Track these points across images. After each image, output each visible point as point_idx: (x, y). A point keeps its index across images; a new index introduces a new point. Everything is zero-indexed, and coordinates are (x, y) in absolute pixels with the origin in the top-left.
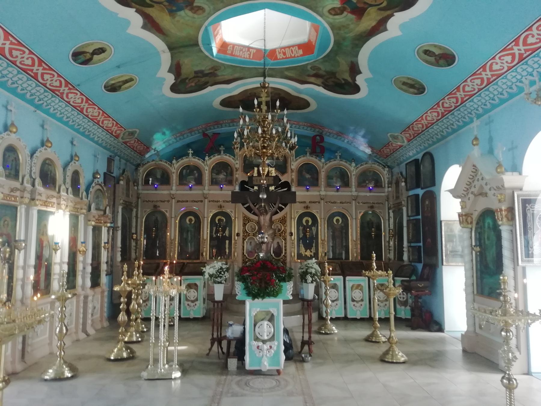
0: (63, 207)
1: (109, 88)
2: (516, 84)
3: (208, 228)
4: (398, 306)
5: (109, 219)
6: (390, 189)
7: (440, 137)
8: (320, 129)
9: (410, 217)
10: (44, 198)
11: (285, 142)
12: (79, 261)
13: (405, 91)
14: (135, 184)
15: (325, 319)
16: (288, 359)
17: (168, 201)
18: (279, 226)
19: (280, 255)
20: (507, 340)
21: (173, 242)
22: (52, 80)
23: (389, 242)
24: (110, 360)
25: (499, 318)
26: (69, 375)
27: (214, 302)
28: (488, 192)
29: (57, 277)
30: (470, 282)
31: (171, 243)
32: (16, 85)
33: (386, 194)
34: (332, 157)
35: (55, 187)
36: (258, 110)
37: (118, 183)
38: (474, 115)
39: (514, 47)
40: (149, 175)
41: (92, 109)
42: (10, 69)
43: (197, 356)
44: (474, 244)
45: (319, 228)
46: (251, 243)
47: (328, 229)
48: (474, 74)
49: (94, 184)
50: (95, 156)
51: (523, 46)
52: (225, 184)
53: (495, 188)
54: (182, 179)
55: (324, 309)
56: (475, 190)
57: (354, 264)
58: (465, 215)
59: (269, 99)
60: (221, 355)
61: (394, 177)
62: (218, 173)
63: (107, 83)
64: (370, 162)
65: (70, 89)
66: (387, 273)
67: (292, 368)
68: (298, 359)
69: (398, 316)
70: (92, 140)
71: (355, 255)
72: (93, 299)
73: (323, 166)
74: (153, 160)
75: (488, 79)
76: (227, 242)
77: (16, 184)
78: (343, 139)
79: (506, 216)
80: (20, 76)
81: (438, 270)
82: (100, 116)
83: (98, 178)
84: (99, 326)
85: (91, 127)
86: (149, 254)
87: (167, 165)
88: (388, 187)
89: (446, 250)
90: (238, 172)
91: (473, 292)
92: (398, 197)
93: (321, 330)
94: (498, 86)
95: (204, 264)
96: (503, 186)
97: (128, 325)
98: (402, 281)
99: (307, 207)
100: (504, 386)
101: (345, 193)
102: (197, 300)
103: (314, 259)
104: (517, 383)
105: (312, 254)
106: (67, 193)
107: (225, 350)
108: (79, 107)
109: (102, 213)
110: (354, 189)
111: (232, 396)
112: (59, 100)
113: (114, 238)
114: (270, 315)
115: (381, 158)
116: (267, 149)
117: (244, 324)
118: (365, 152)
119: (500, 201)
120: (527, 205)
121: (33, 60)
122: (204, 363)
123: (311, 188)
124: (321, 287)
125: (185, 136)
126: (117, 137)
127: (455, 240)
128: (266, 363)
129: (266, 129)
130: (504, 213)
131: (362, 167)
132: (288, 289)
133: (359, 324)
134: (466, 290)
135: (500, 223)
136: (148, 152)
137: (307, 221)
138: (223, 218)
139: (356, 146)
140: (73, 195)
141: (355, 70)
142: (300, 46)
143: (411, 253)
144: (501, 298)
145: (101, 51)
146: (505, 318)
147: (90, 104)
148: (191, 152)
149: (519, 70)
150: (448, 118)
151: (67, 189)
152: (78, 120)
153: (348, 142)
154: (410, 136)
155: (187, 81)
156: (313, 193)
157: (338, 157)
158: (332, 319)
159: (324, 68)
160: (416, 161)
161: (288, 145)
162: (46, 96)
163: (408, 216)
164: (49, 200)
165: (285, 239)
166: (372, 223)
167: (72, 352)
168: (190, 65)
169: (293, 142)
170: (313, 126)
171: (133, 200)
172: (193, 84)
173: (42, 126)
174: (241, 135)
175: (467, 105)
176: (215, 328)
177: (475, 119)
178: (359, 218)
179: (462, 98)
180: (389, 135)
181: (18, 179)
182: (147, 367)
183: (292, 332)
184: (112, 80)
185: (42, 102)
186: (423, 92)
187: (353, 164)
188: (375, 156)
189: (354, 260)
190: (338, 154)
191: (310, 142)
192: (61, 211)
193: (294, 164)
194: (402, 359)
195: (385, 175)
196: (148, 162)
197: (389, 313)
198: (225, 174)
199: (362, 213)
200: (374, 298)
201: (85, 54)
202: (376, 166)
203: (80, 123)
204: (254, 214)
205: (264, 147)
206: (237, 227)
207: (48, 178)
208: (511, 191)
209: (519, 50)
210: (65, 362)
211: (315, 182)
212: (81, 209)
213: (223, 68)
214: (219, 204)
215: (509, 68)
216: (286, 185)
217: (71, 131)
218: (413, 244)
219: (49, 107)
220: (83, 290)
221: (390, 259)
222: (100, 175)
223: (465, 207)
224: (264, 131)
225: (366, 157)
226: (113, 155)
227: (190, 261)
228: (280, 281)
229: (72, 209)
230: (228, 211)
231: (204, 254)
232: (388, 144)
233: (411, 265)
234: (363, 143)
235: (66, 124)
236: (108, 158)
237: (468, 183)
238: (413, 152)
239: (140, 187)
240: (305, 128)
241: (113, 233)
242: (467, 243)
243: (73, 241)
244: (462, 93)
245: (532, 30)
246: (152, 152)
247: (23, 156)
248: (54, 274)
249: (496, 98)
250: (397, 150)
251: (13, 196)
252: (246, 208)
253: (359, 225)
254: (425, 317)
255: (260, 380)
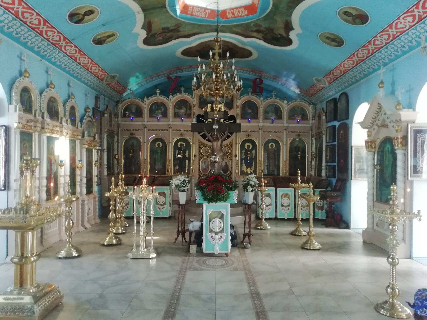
0: (65, 134)
1: (96, 42)
2: (415, 39)
3: (172, 151)
4: (316, 210)
5: (98, 143)
6: (313, 121)
7: (354, 80)
8: (260, 73)
9: (328, 143)
10: (51, 127)
11: (233, 85)
12: (77, 175)
13: (328, 44)
14: (116, 117)
15: (261, 219)
16: (233, 246)
17: (142, 130)
18: (227, 149)
19: (227, 172)
20: (392, 232)
21: (146, 161)
22: (53, 36)
23: (311, 162)
24: (103, 245)
25: (388, 215)
26: (76, 255)
27: (179, 205)
28: (389, 124)
29: (62, 186)
30: (371, 192)
31: (144, 162)
32: (27, 40)
33: (310, 125)
34: (269, 96)
35: (58, 119)
36: (213, 60)
37: (103, 116)
38: (382, 63)
39: (415, 10)
40: (126, 110)
41: (83, 58)
42: (22, 28)
43: (167, 243)
44: (376, 164)
45: (258, 151)
46: (205, 162)
47: (264, 152)
48: (383, 31)
49: (86, 117)
50: (86, 95)
51: (422, 9)
52: (185, 117)
53: (394, 121)
54: (152, 113)
55: (260, 211)
56: (379, 123)
57: (284, 178)
58: (370, 142)
59: (221, 51)
60: (184, 243)
61: (317, 112)
62: (180, 108)
63: (94, 38)
64: (299, 100)
65: (67, 43)
66: (309, 185)
67: (237, 252)
68: (241, 246)
69: (316, 217)
70: (83, 82)
71: (285, 172)
72: (88, 202)
73: (262, 103)
74: (129, 98)
75: (394, 35)
76: (187, 161)
77: (31, 117)
78: (277, 81)
79: (401, 143)
80: (30, 33)
81: (348, 183)
82: (89, 64)
83: (89, 112)
84: (93, 223)
85: (82, 72)
86: (127, 170)
87: (140, 102)
88: (312, 120)
89: (355, 168)
90: (195, 108)
91: (373, 199)
92: (319, 128)
93: (258, 226)
94: (409, 36)
95: (171, 178)
96: (400, 120)
97: (115, 221)
98: (320, 191)
99: (248, 135)
100: (389, 263)
101: (278, 124)
102: (165, 204)
103: (253, 174)
104: (398, 261)
105: (252, 171)
106: (67, 123)
107: (187, 239)
108: (74, 56)
109: (92, 139)
110: (285, 121)
111: (194, 270)
112: (59, 52)
113: (101, 158)
114: (221, 214)
115: (308, 97)
116: (219, 91)
117: (202, 221)
118: (294, 92)
119: (397, 131)
120: (418, 134)
121: (40, 21)
122: (172, 248)
123: (253, 121)
124: (258, 195)
125: (154, 79)
126: (102, 80)
127: (362, 161)
128: (217, 248)
129: (218, 75)
130: (400, 140)
131: (292, 104)
132: (234, 196)
133: (286, 223)
134: (368, 198)
135: (396, 148)
136: (125, 91)
137: (248, 146)
138: (183, 143)
139: (288, 87)
140: (71, 125)
141: (289, 27)
142: (246, 7)
143: (328, 170)
144: (391, 202)
145: (90, 12)
146: (392, 216)
147: (81, 55)
148: (158, 91)
149: (418, 28)
150: (361, 65)
151: (67, 120)
152: (73, 67)
153: (281, 84)
154: (331, 80)
155: (156, 36)
156: (254, 124)
157: (274, 96)
158: (266, 219)
159: (264, 25)
160: (335, 99)
161: (236, 88)
162: (49, 49)
163: (327, 142)
164: (54, 129)
165: (231, 160)
166: (299, 148)
167: (76, 239)
168: (159, 23)
169: (239, 85)
170: (254, 71)
171: (115, 129)
172: (161, 38)
173: (47, 72)
174: (199, 79)
175: (377, 56)
176: (180, 224)
177: (382, 67)
178: (289, 143)
179: (373, 50)
180: (314, 78)
181: (32, 113)
182: (132, 250)
183: (236, 228)
184: (98, 35)
185: (46, 53)
186: (342, 45)
187: (286, 102)
188: (303, 96)
189: (283, 176)
190: (274, 94)
191: (251, 84)
192: (63, 137)
193: (239, 102)
194: (318, 247)
195: (310, 110)
196: (125, 99)
197: (309, 214)
198: (185, 109)
199: (291, 140)
200: (298, 204)
201: (78, 15)
202: (303, 103)
203: (74, 69)
204: (209, 140)
205: (217, 89)
206: (195, 150)
207: (53, 113)
208: (406, 124)
209: (419, 12)
210: (73, 246)
211: (255, 116)
212: (78, 136)
213: (184, 25)
214: (180, 132)
215: (411, 27)
216: (233, 118)
217: (68, 76)
218: (329, 164)
219: (52, 57)
220: (81, 196)
221: (311, 175)
222: (90, 109)
223: (371, 136)
224: (216, 77)
225: (295, 96)
226: (99, 94)
227: (159, 176)
228: (228, 190)
229: (71, 135)
230: (187, 138)
231: (170, 170)
232: (313, 86)
233: (327, 179)
234: (294, 85)
235: (64, 70)
236: (95, 96)
237: (374, 117)
238: (333, 93)
239: (120, 119)
240: (248, 72)
241: (101, 154)
242: (370, 163)
243: (73, 160)
244: (373, 46)
245: (400, 19)
246: (129, 92)
247: (35, 95)
248: (60, 184)
249: (399, 50)
250: (320, 90)
251: (29, 126)
252: (201, 136)
253: (288, 149)
254: (337, 218)
255: (213, 260)
